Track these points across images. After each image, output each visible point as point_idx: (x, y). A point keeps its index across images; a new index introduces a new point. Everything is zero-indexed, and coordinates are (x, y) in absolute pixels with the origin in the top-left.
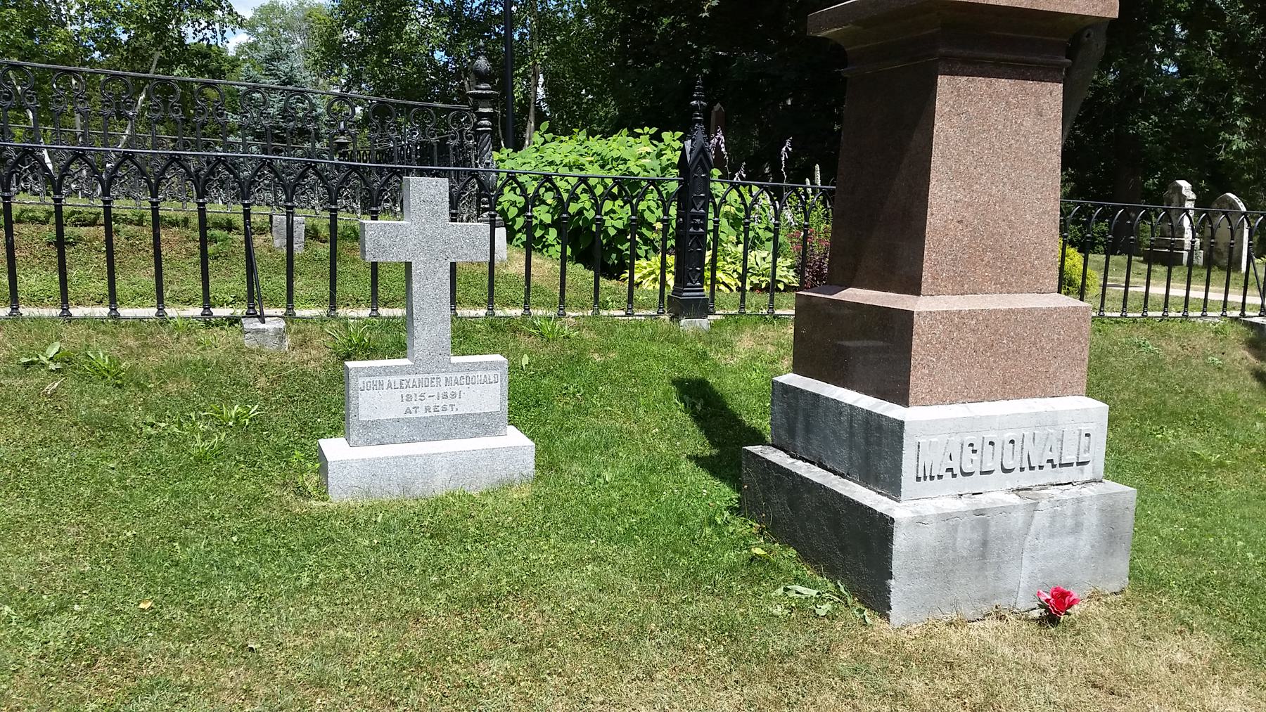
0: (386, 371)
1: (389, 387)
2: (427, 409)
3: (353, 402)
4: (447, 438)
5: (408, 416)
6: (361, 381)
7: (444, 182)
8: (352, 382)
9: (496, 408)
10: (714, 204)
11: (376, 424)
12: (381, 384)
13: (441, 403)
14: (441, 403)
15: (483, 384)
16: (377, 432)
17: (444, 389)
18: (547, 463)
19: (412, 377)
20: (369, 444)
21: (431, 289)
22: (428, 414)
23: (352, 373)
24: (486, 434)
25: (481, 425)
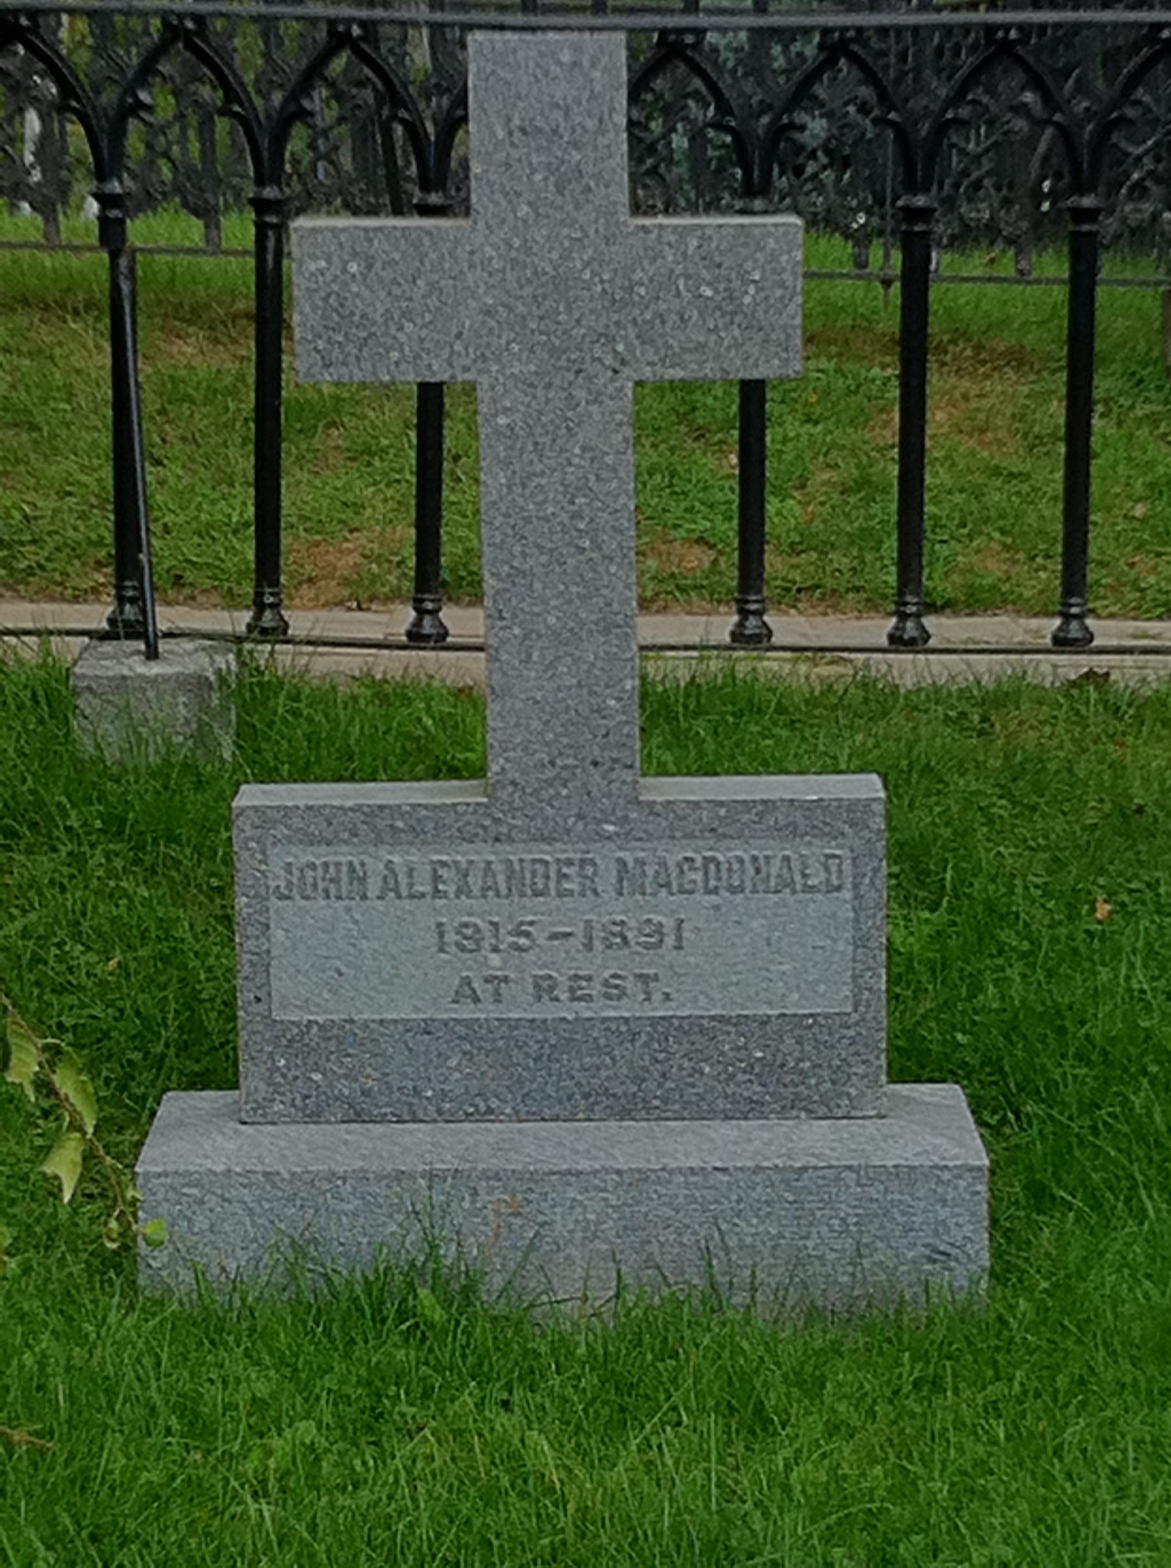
0: (379, 826)
1: (390, 885)
2: (544, 989)
3: (247, 941)
4: (625, 1114)
5: (466, 1012)
6: (279, 857)
7: (158, 609)
8: (245, 862)
9: (835, 998)
10: (414, 132)
11: (341, 1035)
12: (358, 877)
13: (601, 965)
14: (601, 965)
15: (782, 908)
16: (351, 1077)
17: (614, 909)
18: (1024, 1193)
19: (481, 853)
20: (315, 1117)
21: (555, 480)
22: (546, 1011)
23: (243, 829)
24: (796, 1105)
25: (773, 1069)
